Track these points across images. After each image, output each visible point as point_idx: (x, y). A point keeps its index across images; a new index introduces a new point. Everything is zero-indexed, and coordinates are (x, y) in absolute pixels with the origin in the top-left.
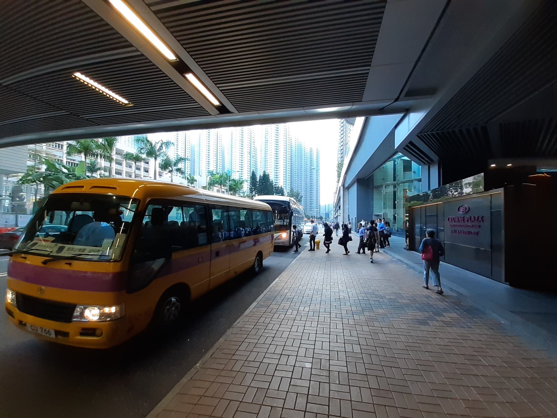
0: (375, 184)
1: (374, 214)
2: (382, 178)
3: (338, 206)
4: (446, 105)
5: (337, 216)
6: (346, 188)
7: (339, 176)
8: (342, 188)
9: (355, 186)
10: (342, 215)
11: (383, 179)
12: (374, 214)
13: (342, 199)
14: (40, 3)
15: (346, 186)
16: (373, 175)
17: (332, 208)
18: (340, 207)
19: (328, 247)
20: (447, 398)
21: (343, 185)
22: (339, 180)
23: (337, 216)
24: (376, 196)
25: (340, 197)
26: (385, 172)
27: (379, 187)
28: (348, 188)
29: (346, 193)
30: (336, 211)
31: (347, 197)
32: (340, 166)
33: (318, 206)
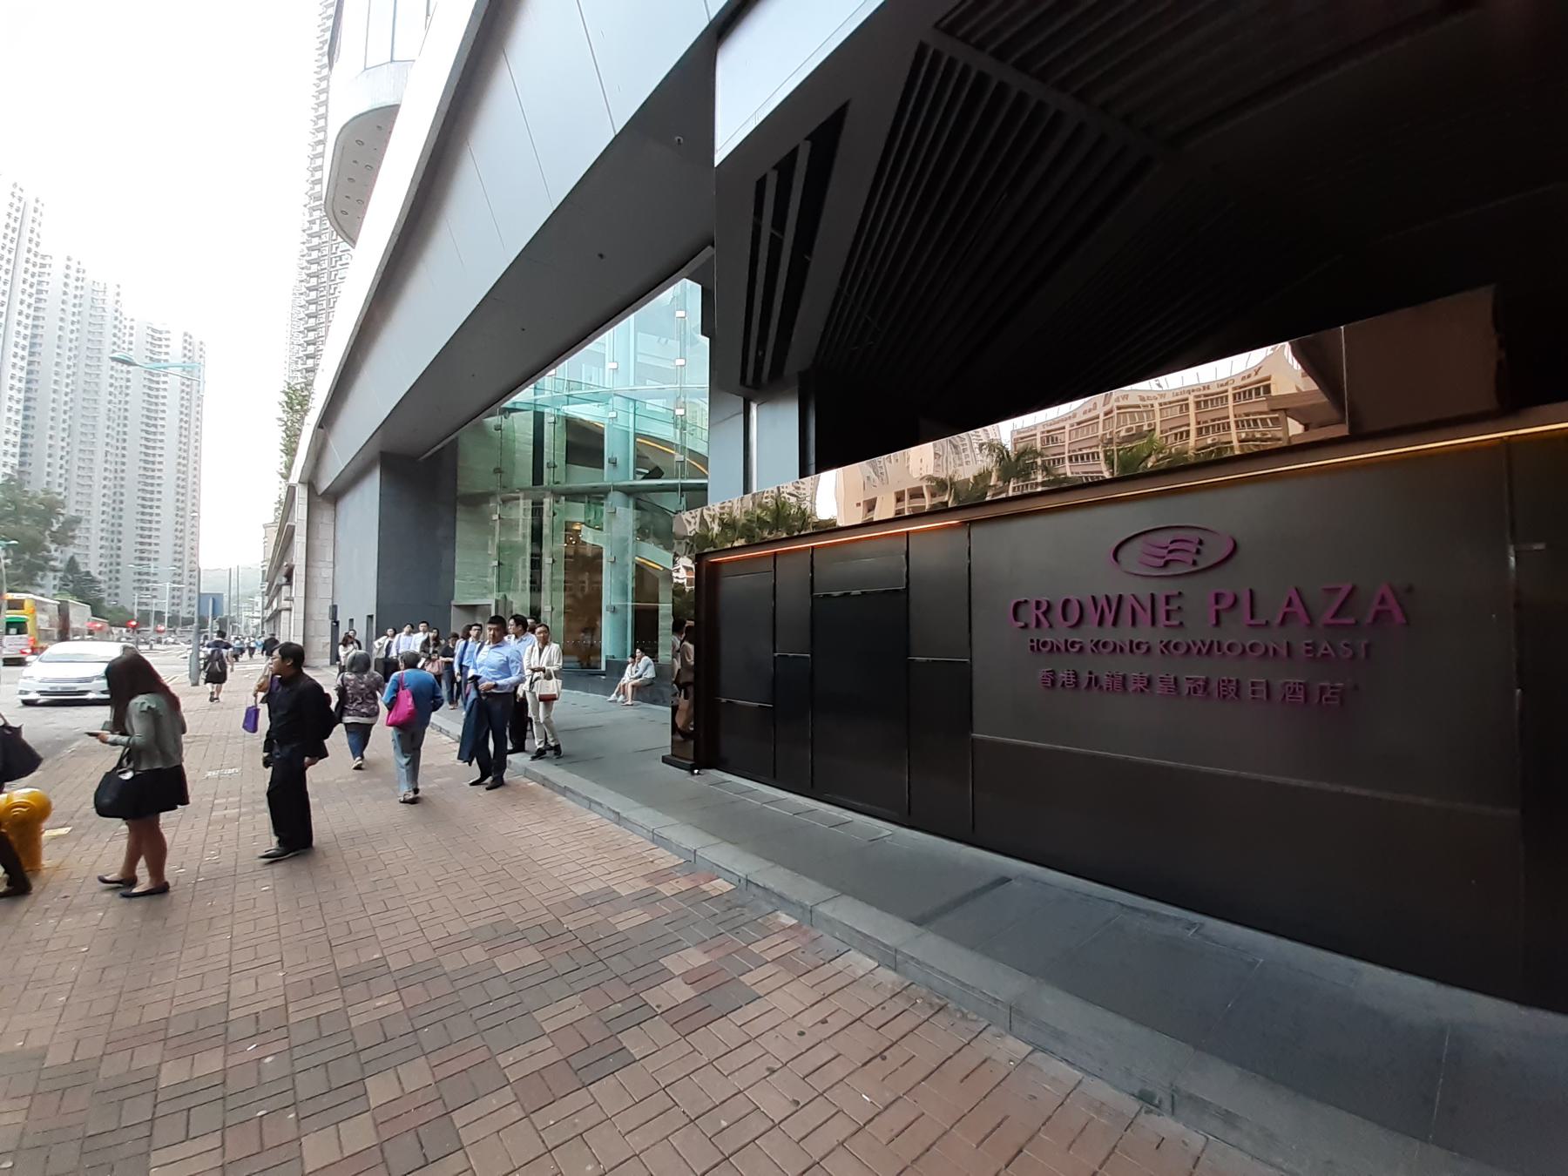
0: (463, 488)
1: (459, 599)
2: (495, 466)
3: (280, 572)
4: (839, 293)
5: (277, 613)
6: (325, 497)
7: (290, 451)
8: (302, 494)
9: (372, 487)
10: (299, 605)
11: (498, 471)
12: (459, 599)
13: (300, 540)
14: (991, 7)
15: (324, 484)
16: (455, 441)
17: (254, 581)
18: (289, 576)
19: (147, 844)
20: (886, 1108)
21: (310, 484)
22: (289, 467)
23: (277, 613)
24: (464, 533)
25: (292, 530)
26: (504, 446)
27: (477, 501)
28: (335, 496)
29: (325, 516)
30: (273, 591)
31: (325, 532)
32: (296, 401)
33: (196, 572)
